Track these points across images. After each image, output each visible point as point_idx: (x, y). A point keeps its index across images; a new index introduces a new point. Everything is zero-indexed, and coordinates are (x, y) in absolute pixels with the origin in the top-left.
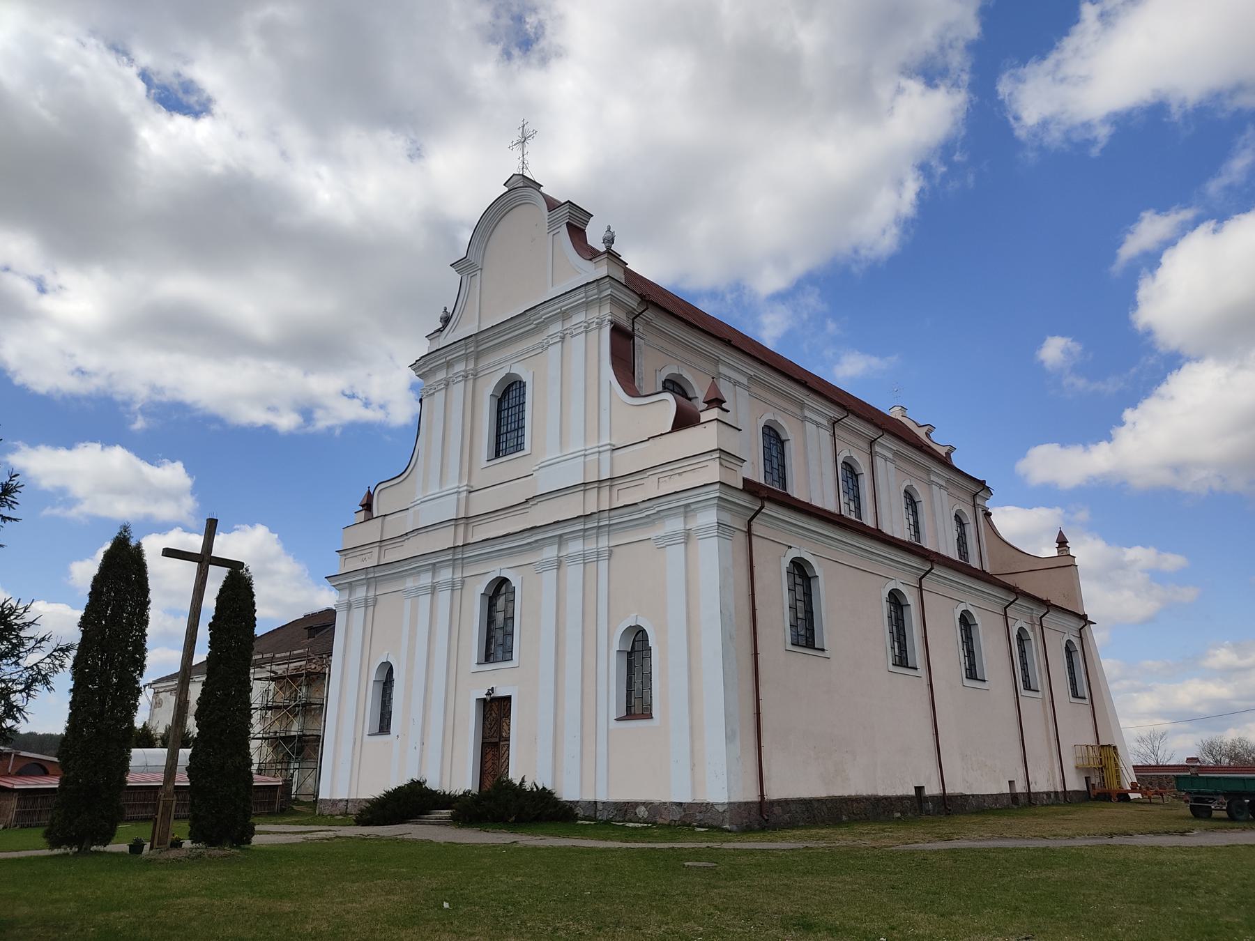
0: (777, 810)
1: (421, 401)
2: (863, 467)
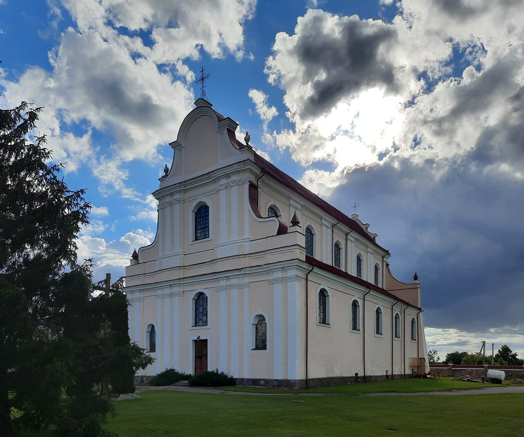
0: (311, 382)
2: (343, 246)
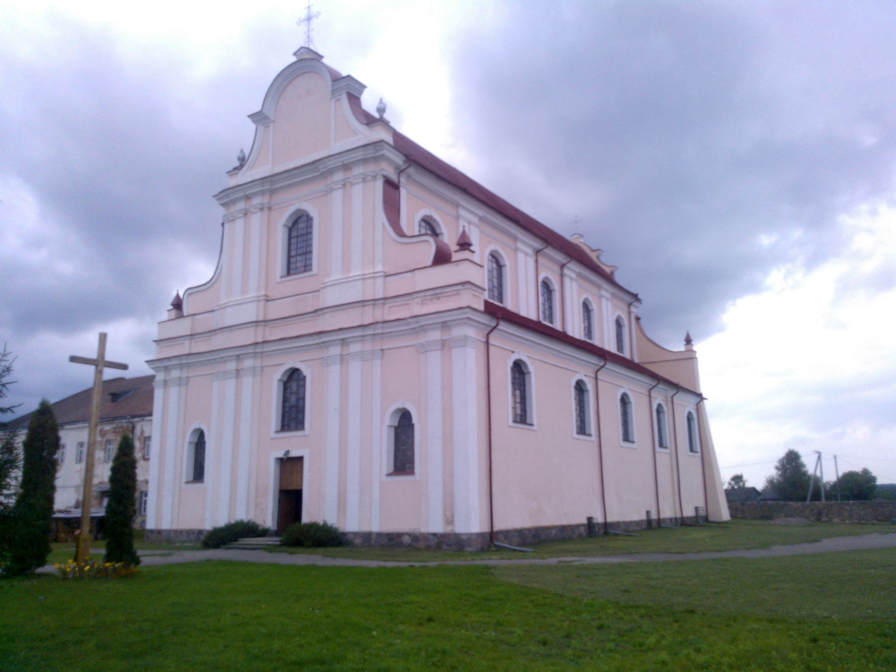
1: (223, 224)
2: (556, 286)
